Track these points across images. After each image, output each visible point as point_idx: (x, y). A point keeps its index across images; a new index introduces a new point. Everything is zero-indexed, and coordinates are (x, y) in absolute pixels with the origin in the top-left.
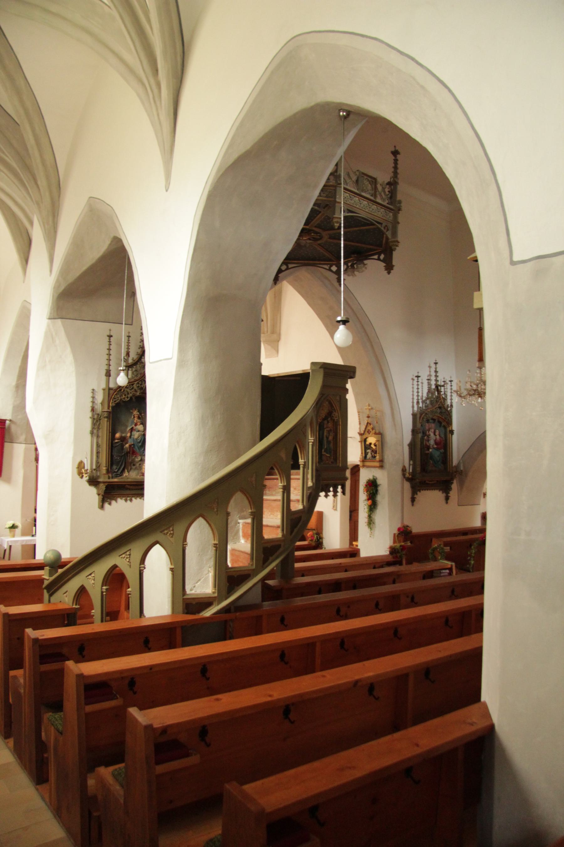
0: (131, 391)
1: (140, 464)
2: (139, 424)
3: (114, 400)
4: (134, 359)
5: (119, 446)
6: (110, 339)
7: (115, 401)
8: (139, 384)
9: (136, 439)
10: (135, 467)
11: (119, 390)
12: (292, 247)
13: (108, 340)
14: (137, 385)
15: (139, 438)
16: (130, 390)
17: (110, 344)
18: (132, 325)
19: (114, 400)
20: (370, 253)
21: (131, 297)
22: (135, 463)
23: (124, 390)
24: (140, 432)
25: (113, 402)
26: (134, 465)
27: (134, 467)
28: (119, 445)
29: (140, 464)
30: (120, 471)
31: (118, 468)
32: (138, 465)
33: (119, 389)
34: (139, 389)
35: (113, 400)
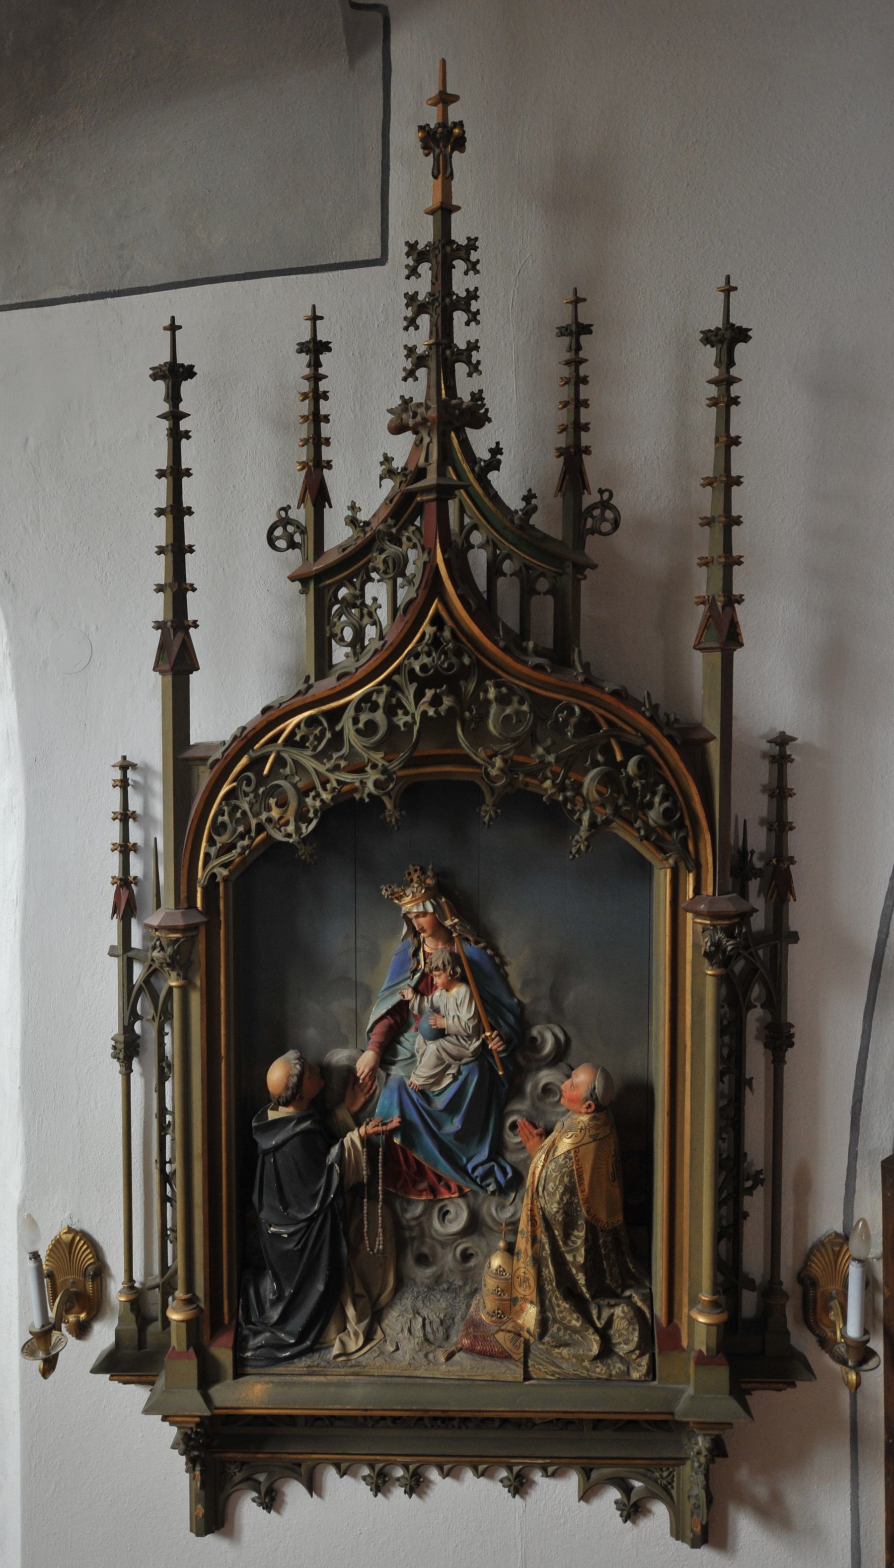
0: (322, 769)
1: (466, 1256)
2: (439, 979)
3: (220, 840)
4: (363, 516)
5: (286, 1149)
6: (174, 397)
7: (228, 848)
8: (374, 707)
9: (423, 1092)
10: (429, 1271)
11: (245, 769)
12: (717, 1340)
13: (165, 408)
14: (364, 718)
15: (447, 1081)
16: (318, 757)
17: (177, 436)
18: (382, 261)
19: (220, 840)
20: (775, 896)
21: (355, 51)
22: (426, 1250)
23: (280, 762)
24: (443, 1042)
25: (213, 851)
26: (423, 1260)
27: (424, 1274)
28: (284, 1143)
29: (466, 1256)
30: (298, 1322)
31: (288, 1292)
32: (449, 1259)
33: (244, 761)
34: (375, 748)
35: (211, 842)
